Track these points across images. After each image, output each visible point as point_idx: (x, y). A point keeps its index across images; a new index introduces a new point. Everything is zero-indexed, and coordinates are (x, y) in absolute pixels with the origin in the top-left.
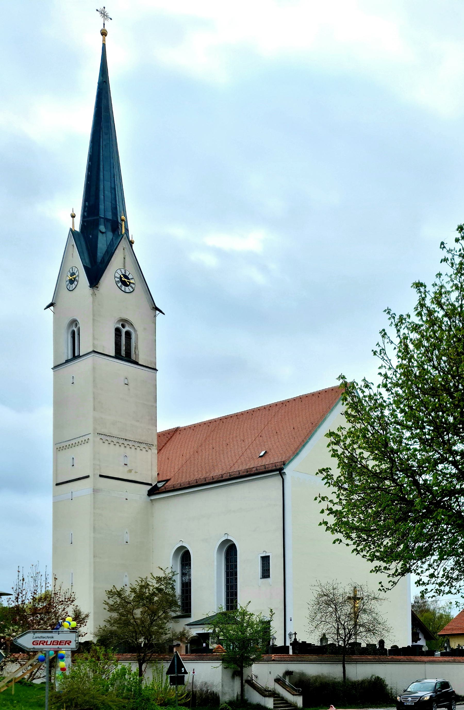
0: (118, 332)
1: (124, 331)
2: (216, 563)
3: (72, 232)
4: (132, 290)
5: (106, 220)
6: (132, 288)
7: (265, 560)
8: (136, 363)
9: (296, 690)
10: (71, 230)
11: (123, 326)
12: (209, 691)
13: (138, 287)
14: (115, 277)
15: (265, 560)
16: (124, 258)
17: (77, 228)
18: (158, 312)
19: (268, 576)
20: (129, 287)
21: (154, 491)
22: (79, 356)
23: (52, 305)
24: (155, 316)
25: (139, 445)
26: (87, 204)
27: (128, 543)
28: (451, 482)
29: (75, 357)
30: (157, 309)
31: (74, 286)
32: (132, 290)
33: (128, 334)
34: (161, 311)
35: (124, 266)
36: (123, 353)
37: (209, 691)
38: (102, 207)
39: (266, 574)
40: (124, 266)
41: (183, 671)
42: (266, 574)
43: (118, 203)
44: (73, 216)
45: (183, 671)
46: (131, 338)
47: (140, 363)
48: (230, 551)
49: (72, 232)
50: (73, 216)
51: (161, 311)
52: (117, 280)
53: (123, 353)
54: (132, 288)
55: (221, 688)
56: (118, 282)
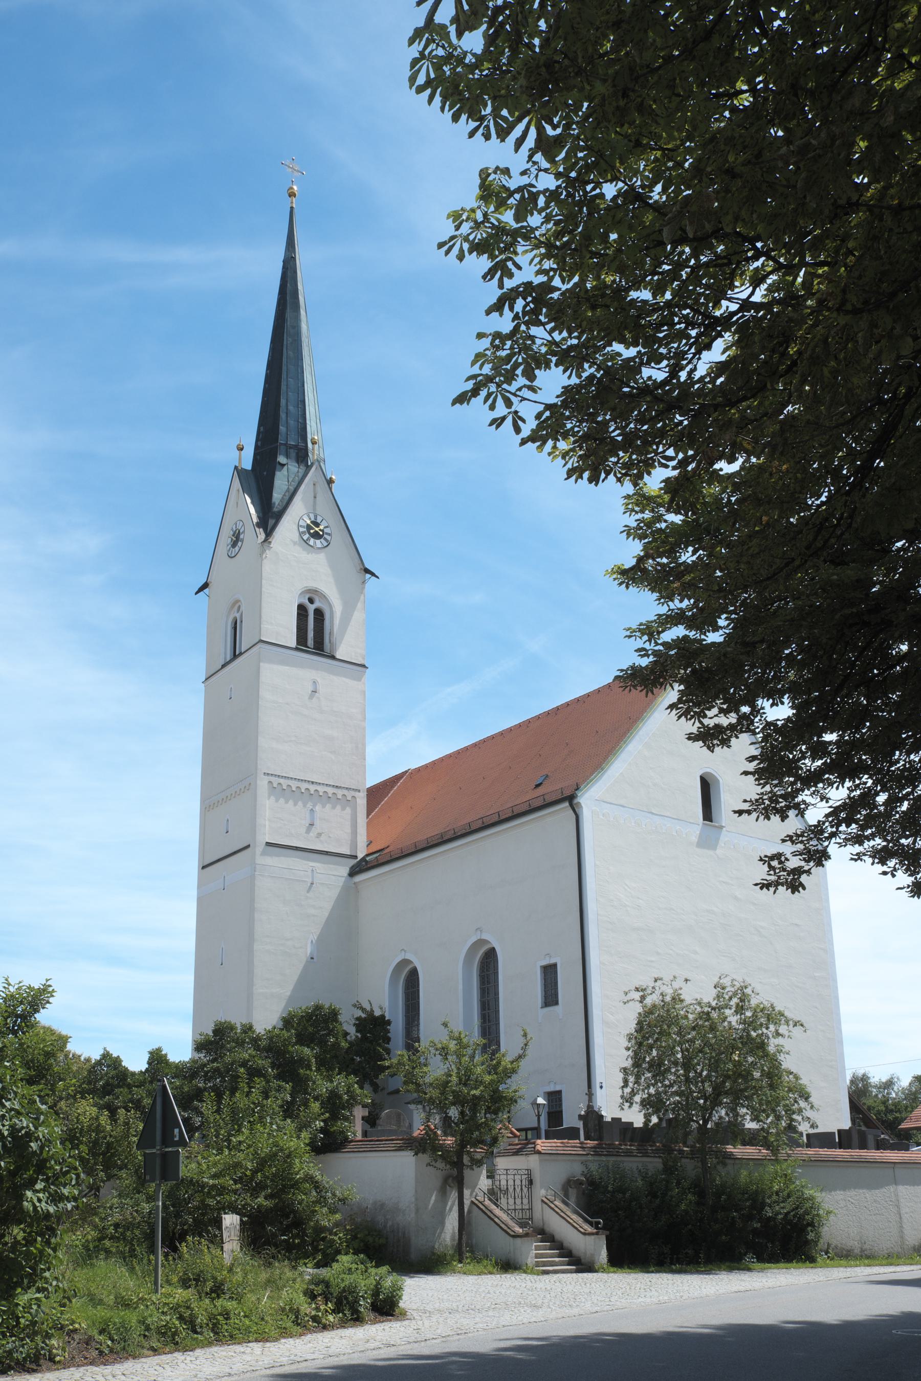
0: (302, 609)
1: (311, 608)
2: (461, 987)
3: (239, 471)
4: (326, 544)
5: (288, 447)
6: (326, 540)
7: (550, 972)
8: (333, 657)
9: (591, 1224)
10: (236, 468)
11: (311, 601)
12: (390, 1223)
13: (337, 537)
14: (299, 526)
15: (550, 972)
16: (315, 497)
17: (248, 465)
18: (368, 576)
19: (556, 1003)
20: (322, 540)
21: (359, 868)
22: (241, 654)
23: (205, 586)
24: (364, 582)
25: (335, 790)
26: (262, 429)
27: (315, 960)
28: (882, 769)
29: (235, 656)
30: (367, 571)
31: (237, 548)
32: (326, 544)
33: (319, 613)
34: (373, 574)
35: (314, 509)
36: (310, 642)
37: (390, 1223)
38: (282, 429)
39: (550, 998)
40: (314, 509)
41: (177, 1139)
42: (550, 998)
43: (308, 422)
44: (241, 449)
45: (177, 1139)
46: (323, 620)
47: (338, 657)
48: (487, 965)
49: (239, 471)
50: (241, 449)
51: (373, 574)
52: (302, 530)
53: (310, 642)
54: (326, 540)
55: (413, 1215)
56: (304, 533)
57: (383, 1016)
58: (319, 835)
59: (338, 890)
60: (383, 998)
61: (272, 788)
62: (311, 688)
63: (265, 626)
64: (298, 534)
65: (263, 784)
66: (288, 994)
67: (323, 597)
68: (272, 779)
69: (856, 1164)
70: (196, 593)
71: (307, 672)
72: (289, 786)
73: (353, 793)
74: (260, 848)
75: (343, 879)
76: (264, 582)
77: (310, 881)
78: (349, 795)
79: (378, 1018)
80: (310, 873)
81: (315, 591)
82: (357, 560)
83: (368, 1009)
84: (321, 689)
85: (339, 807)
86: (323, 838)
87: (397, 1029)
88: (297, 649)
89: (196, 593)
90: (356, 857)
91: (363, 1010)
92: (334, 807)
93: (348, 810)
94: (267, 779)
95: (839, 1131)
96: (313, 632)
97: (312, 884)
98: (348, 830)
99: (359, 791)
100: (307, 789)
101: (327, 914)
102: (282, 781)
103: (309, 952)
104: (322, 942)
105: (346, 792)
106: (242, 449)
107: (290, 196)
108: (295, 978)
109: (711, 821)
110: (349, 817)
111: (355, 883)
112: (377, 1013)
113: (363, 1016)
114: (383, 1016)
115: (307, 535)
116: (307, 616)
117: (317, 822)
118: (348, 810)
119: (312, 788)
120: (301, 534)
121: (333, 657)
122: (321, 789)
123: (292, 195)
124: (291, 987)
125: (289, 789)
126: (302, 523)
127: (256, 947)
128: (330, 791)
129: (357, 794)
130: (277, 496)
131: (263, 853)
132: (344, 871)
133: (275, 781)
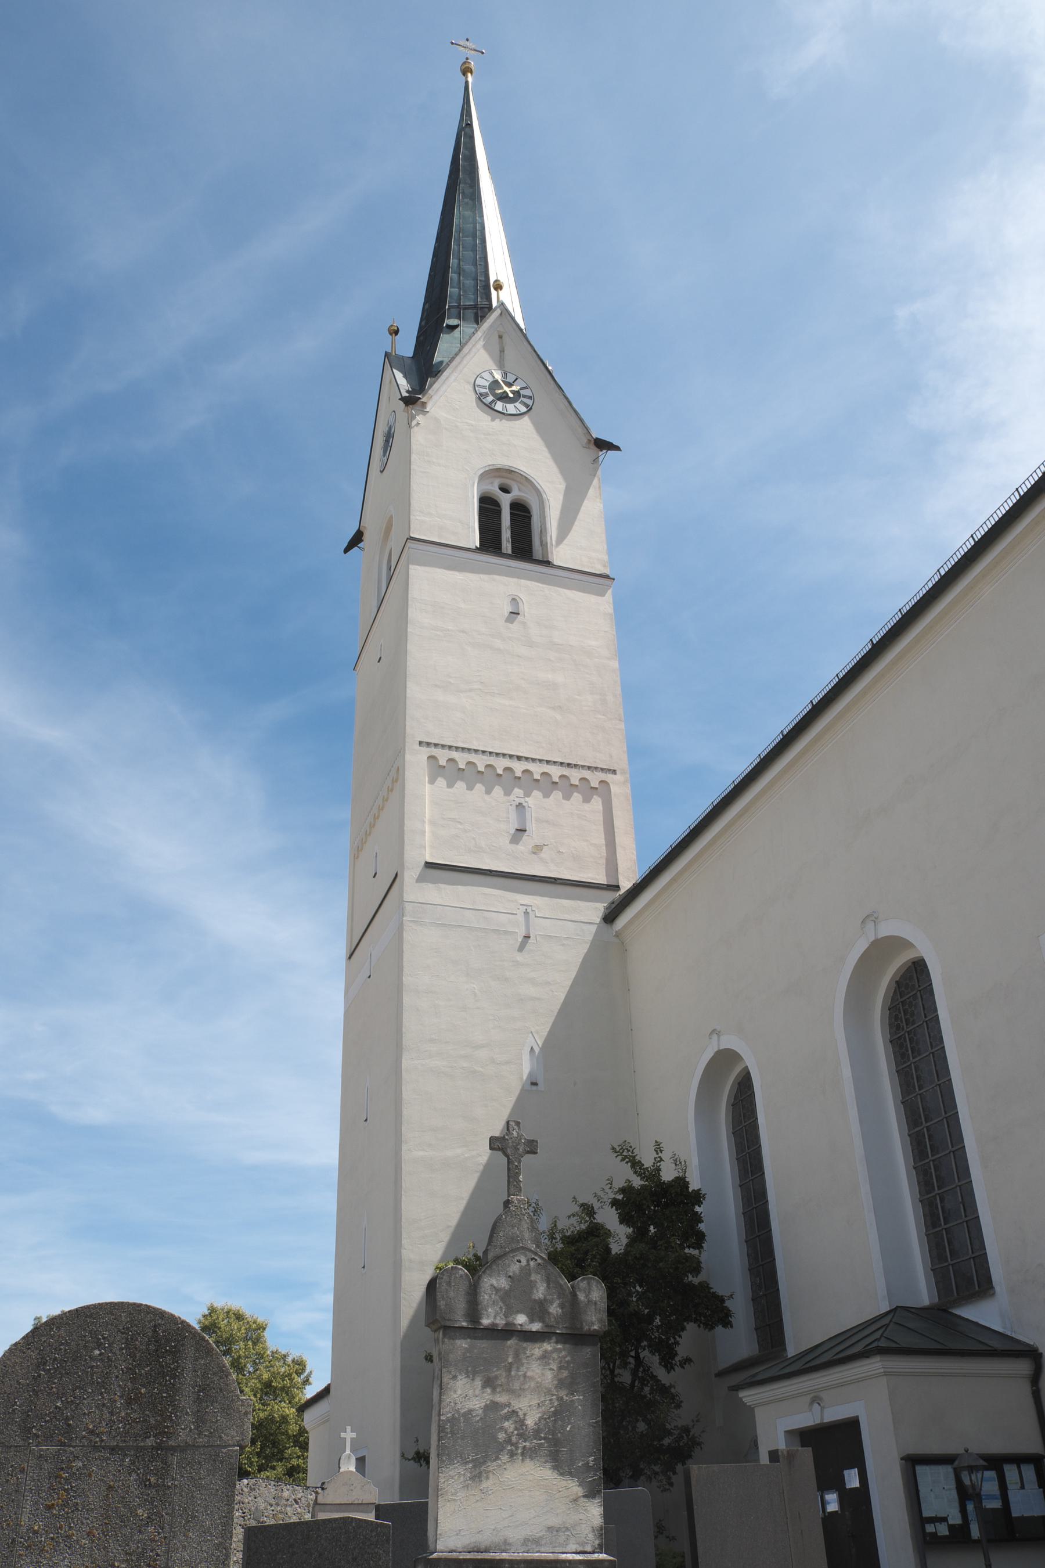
1: (505, 501)
10: (387, 355)
25: (565, 771)
27: (541, 1087)
36: (507, 546)
57: (681, 1183)
58: (538, 849)
59: (584, 949)
60: (683, 1142)
61: (436, 769)
62: (508, 608)
63: (416, 518)
65: (416, 761)
67: (526, 480)
70: (346, 551)
71: (503, 583)
73: (603, 776)
74: (411, 874)
75: (593, 929)
76: (414, 457)
77: (521, 932)
79: (670, 1184)
80: (521, 917)
81: (510, 472)
82: (580, 430)
83: (648, 1162)
84: (525, 608)
86: (545, 854)
87: (721, 1212)
88: (478, 550)
89: (346, 551)
90: (617, 888)
91: (636, 1164)
93: (597, 803)
94: (425, 752)
95: (427, 1503)
96: (509, 529)
97: (527, 937)
98: (601, 840)
99: (614, 772)
101: (562, 996)
102: (455, 755)
103: (526, 1071)
104: (554, 1050)
105: (586, 774)
106: (396, 332)
111: (617, 935)
112: (668, 1175)
113: (637, 1182)
114: (681, 1183)
116: (498, 513)
117: (531, 826)
118: (597, 803)
119: (519, 767)
120: (480, 397)
121: (547, 563)
122: (537, 770)
126: (479, 381)
127: (405, 1063)
128: (556, 772)
129: (609, 777)
131: (421, 879)
132: (594, 910)
133: (443, 756)
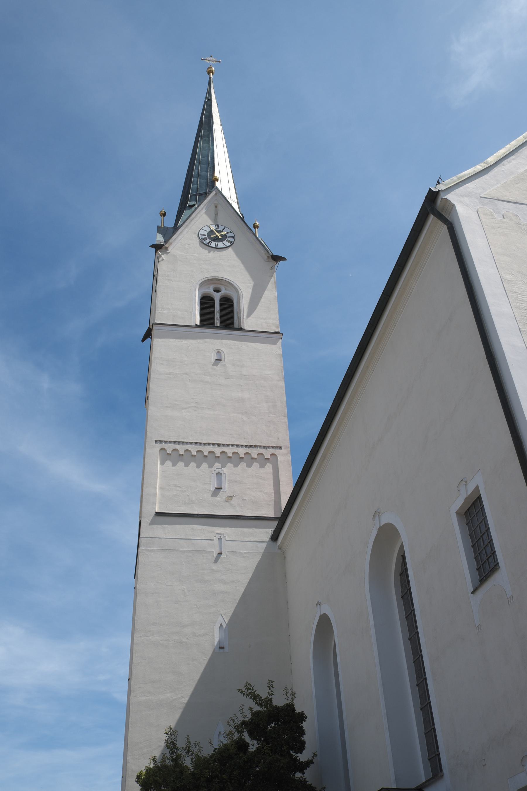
1: (217, 297)
20: (206, 233)
25: (248, 450)
27: (226, 650)
58: (229, 499)
62: (214, 357)
64: (198, 240)
66: (186, 700)
67: (229, 284)
68: (164, 445)
69: (188, 221)
72: (175, 450)
73: (272, 451)
75: (264, 545)
77: (217, 551)
78: (267, 453)
80: (216, 542)
81: (219, 280)
85: (205, 466)
86: (234, 502)
92: (187, 465)
93: (269, 468)
94: (159, 446)
97: (220, 554)
99: (280, 448)
100: (186, 451)
104: (235, 625)
105: (262, 451)
107: (209, 73)
108: (197, 676)
109: (479, 498)
110: (271, 476)
115: (208, 240)
117: (226, 485)
118: (269, 468)
121: (241, 329)
123: (210, 72)
124: (190, 690)
125: (178, 454)
126: (202, 232)
128: (242, 451)
130: (180, 223)
131: (152, 523)
133: (170, 448)
